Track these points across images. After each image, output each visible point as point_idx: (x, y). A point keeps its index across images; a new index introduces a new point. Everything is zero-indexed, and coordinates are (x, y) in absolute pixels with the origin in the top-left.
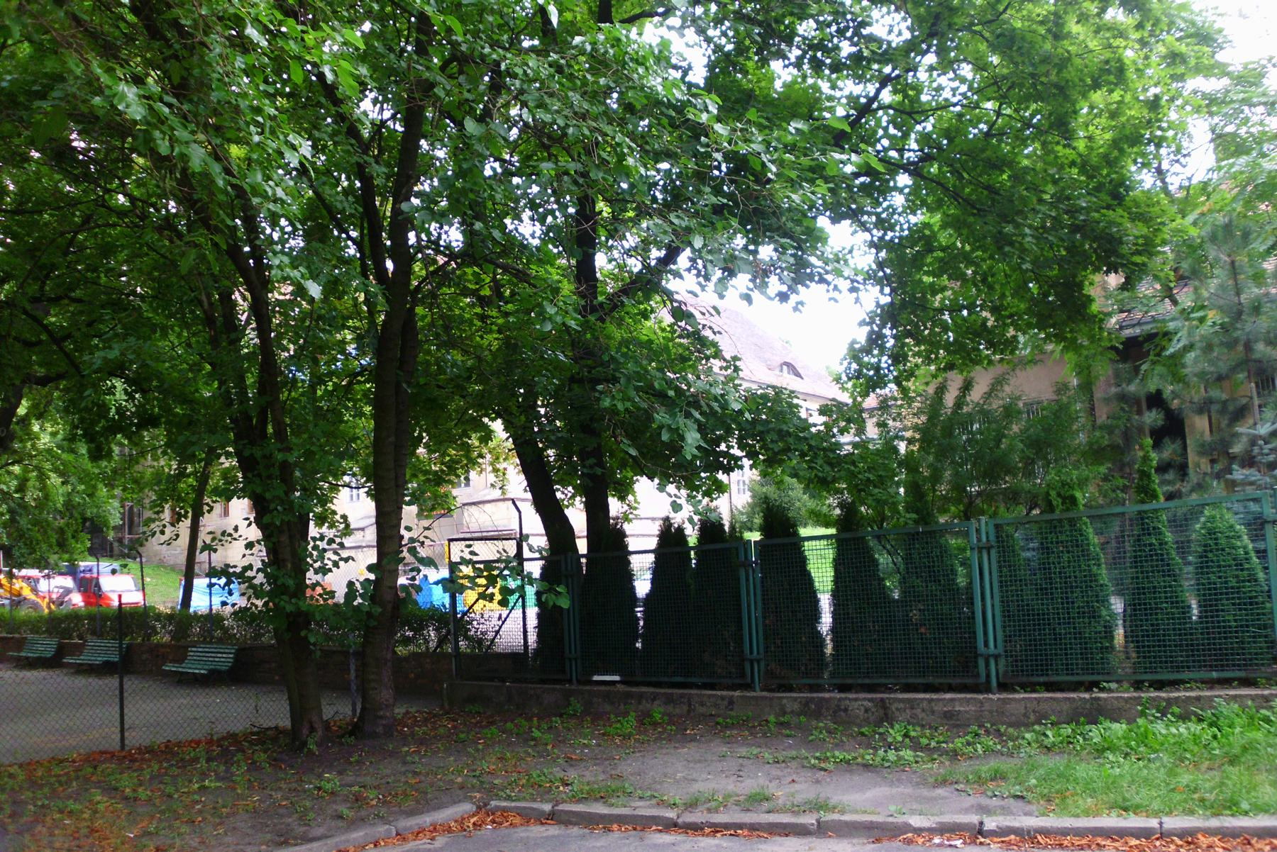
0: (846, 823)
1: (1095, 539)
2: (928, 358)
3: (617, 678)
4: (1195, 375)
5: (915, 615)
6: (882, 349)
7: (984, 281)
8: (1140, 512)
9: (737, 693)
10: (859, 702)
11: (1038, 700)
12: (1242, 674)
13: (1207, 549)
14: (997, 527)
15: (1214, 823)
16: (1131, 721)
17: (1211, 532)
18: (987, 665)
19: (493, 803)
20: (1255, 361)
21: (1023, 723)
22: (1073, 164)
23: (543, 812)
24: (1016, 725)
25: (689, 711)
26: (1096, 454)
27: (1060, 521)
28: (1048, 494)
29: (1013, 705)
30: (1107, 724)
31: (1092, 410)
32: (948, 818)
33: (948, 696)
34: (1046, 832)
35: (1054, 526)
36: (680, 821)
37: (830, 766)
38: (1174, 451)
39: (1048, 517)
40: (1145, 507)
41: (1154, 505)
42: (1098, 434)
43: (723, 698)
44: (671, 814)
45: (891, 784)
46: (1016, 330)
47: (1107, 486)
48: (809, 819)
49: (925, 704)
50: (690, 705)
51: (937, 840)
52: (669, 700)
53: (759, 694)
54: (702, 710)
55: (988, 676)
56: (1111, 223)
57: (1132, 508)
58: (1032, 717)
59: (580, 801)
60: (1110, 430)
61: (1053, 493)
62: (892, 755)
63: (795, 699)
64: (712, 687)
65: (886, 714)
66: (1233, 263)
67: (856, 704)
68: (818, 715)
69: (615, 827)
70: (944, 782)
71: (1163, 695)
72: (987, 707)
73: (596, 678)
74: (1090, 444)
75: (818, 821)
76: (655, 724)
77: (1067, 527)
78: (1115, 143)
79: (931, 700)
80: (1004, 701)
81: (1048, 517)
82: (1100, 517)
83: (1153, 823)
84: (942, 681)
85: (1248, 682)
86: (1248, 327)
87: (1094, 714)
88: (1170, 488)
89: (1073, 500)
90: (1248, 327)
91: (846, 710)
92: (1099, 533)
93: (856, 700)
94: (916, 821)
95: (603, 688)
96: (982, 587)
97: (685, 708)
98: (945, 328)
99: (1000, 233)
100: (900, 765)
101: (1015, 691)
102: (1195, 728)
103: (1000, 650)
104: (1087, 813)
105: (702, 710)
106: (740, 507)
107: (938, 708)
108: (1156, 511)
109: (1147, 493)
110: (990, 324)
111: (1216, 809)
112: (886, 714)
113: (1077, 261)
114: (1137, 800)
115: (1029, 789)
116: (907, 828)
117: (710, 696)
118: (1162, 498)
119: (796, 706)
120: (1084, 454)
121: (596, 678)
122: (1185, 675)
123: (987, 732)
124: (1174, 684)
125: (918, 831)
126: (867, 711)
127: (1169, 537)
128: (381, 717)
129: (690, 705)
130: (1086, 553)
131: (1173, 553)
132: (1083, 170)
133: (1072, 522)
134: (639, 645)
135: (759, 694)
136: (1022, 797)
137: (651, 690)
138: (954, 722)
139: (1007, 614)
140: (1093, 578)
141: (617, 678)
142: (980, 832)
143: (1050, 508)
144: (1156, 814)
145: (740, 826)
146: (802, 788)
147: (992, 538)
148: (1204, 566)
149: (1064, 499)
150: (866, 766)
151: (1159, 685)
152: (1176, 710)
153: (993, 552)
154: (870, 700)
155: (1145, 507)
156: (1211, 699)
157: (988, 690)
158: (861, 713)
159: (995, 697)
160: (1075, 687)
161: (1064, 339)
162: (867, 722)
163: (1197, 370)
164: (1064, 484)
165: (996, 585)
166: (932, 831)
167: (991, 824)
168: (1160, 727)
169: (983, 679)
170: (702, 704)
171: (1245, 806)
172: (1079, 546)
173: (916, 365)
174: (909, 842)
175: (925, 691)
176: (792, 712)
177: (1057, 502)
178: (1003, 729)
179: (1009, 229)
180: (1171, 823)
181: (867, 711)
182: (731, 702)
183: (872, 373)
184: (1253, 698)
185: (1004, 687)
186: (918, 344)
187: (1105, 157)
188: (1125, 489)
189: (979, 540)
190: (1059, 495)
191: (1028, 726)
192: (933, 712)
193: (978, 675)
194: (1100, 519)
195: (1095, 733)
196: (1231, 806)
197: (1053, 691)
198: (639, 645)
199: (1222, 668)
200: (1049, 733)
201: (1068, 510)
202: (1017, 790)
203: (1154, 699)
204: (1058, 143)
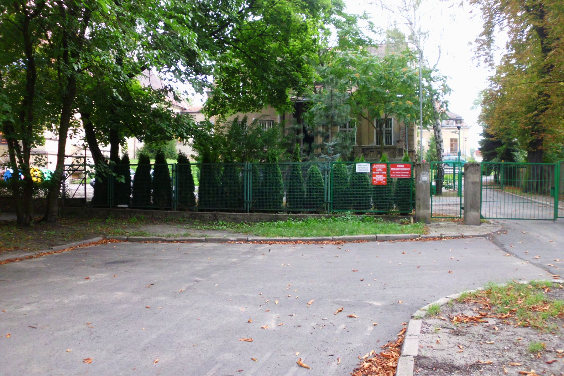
0: (213, 239)
1: (279, 170)
2: (233, 107)
3: (127, 206)
4: (316, 123)
5: (226, 190)
6: (218, 102)
7: (255, 85)
8: (293, 164)
9: (169, 211)
10: (207, 215)
11: (261, 215)
12: (315, 210)
13: (310, 176)
14: (253, 165)
15: (302, 238)
16: (286, 221)
17: (312, 172)
18: (247, 205)
19: (108, 237)
20: (334, 122)
21: (256, 221)
22: (288, 53)
23: (124, 239)
24: (255, 222)
25: (152, 217)
26: (283, 145)
27: (271, 165)
28: (268, 157)
29: (254, 216)
30: (279, 222)
31: (284, 132)
32: (239, 238)
33: (235, 213)
34: (264, 240)
35: (268, 166)
36: (167, 239)
37: (204, 229)
38: (306, 147)
39: (267, 163)
40: (295, 163)
41: (297, 163)
42: (284, 139)
43: (164, 213)
44: (164, 238)
45: (222, 233)
46: (263, 102)
47: (285, 156)
48: (204, 238)
49: (228, 216)
50: (152, 215)
51: (237, 242)
52: (145, 213)
53: (175, 211)
54: (157, 216)
55: (247, 208)
56: (297, 77)
57: (291, 163)
58: (259, 220)
59: (134, 236)
60: (288, 138)
61: (270, 157)
62: (220, 227)
63: (188, 213)
64: (158, 209)
65: (216, 218)
66: (332, 91)
67: (207, 215)
68: (194, 218)
69: (148, 242)
70: (236, 232)
71: (295, 215)
72: (246, 217)
73: (119, 206)
74: (282, 142)
75: (206, 239)
76: (142, 221)
77: (273, 167)
78: (301, 49)
79: (229, 215)
80: (251, 215)
81: (267, 163)
82: (282, 165)
83: (289, 238)
84: (232, 209)
85: (316, 213)
86: (333, 111)
87: (276, 219)
88: (304, 158)
89: (275, 159)
90: (333, 111)
91: (204, 217)
92: (282, 170)
93: (207, 214)
94: (231, 239)
95: (121, 209)
96: (247, 182)
97: (151, 216)
98: (240, 98)
99: (263, 75)
100: (223, 229)
101: (253, 213)
102: (301, 222)
103: (251, 200)
104: (273, 237)
105: (157, 216)
106: (139, 148)
107: (232, 217)
108: (298, 164)
109: (296, 159)
110: (254, 99)
111: (302, 236)
112: (216, 218)
113: (285, 84)
114: (285, 234)
115: (259, 233)
116: (229, 240)
117: (159, 212)
118: (300, 161)
119: (188, 215)
120: (279, 145)
121: (119, 206)
122: (301, 210)
123: (246, 223)
124: (299, 212)
125: (232, 241)
126: (210, 217)
127: (301, 172)
128: (54, 215)
129: (152, 215)
130: (277, 175)
131: (302, 177)
132: (291, 55)
133: (274, 165)
134: (131, 196)
135: (175, 211)
136: (257, 235)
137: (139, 210)
138: (236, 220)
139: (253, 191)
140: (279, 182)
141: (127, 206)
142: (247, 241)
143: (268, 161)
144: (289, 237)
145: (184, 240)
146: (198, 233)
147: (251, 168)
148: (309, 181)
149: (273, 158)
150: (214, 230)
151: (294, 212)
152: (298, 219)
153: (251, 173)
154: (211, 214)
155: (295, 163)
156: (307, 216)
157: (247, 212)
158: (208, 218)
159: (249, 214)
160: (272, 212)
161: (278, 107)
162: (210, 220)
163: (317, 122)
164: (273, 154)
165: (251, 183)
166: (235, 241)
167: (250, 239)
168: (293, 223)
169: (245, 209)
170: (157, 215)
171: (309, 235)
172: (275, 172)
173: (228, 109)
174: (230, 243)
175: (228, 212)
176: (187, 217)
177: (270, 159)
178: (250, 223)
179: (265, 75)
180: (292, 238)
181: (210, 217)
182: (167, 214)
183: (213, 109)
184: (317, 216)
185: (251, 212)
186: (230, 102)
187: (298, 52)
188: (290, 157)
189: (247, 168)
190: (271, 157)
191: (258, 222)
192: (230, 218)
193: (244, 208)
194: (282, 165)
195: (276, 224)
196: (306, 235)
197: (265, 213)
198: (131, 196)
199: (311, 208)
200: (263, 224)
201: (273, 162)
202: (256, 233)
203: (292, 216)
204: (284, 46)
